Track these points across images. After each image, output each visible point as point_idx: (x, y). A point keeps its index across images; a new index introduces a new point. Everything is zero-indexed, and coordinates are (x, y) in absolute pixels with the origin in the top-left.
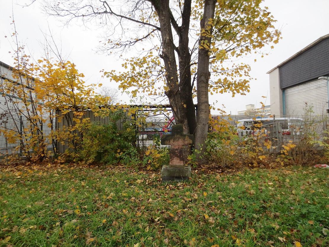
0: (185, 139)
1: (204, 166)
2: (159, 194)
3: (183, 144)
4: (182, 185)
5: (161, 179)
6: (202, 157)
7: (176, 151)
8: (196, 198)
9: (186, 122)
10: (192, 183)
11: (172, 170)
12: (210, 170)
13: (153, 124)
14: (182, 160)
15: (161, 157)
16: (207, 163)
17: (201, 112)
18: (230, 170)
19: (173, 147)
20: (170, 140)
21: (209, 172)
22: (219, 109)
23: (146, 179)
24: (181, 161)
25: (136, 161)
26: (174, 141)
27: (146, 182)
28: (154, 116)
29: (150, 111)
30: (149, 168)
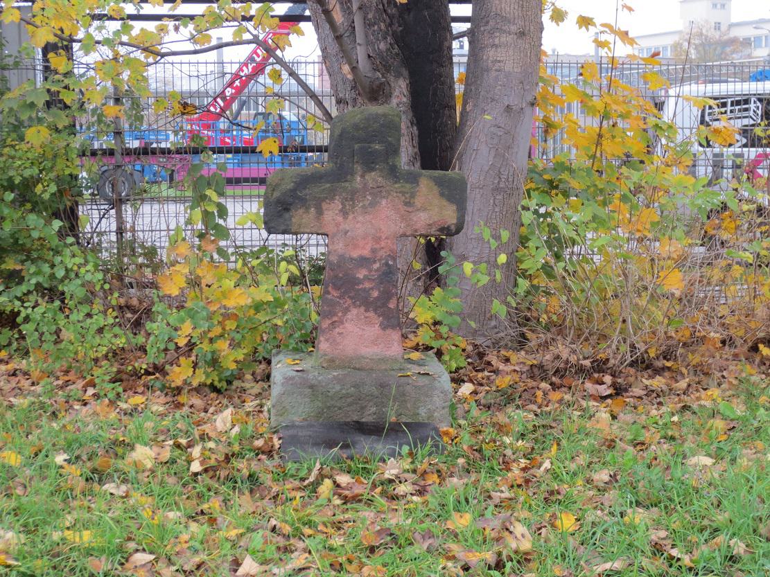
0: (413, 196)
1: (507, 360)
2: (287, 529)
3: (401, 227)
4: (407, 475)
5: (277, 443)
6: (505, 308)
7: (361, 274)
8: (526, 545)
9: (400, 90)
10: (468, 457)
11: (338, 387)
12: (544, 385)
13: (185, 105)
14: (393, 327)
15: (258, 307)
16: (522, 341)
17: (491, 33)
18: (658, 382)
19: (340, 247)
20: (324, 206)
21: (539, 393)
22: (585, 22)
23: (183, 441)
24: (389, 331)
25: (100, 331)
26: (344, 213)
27: (189, 462)
28: (195, 52)
29: (171, 24)
30: (180, 373)
